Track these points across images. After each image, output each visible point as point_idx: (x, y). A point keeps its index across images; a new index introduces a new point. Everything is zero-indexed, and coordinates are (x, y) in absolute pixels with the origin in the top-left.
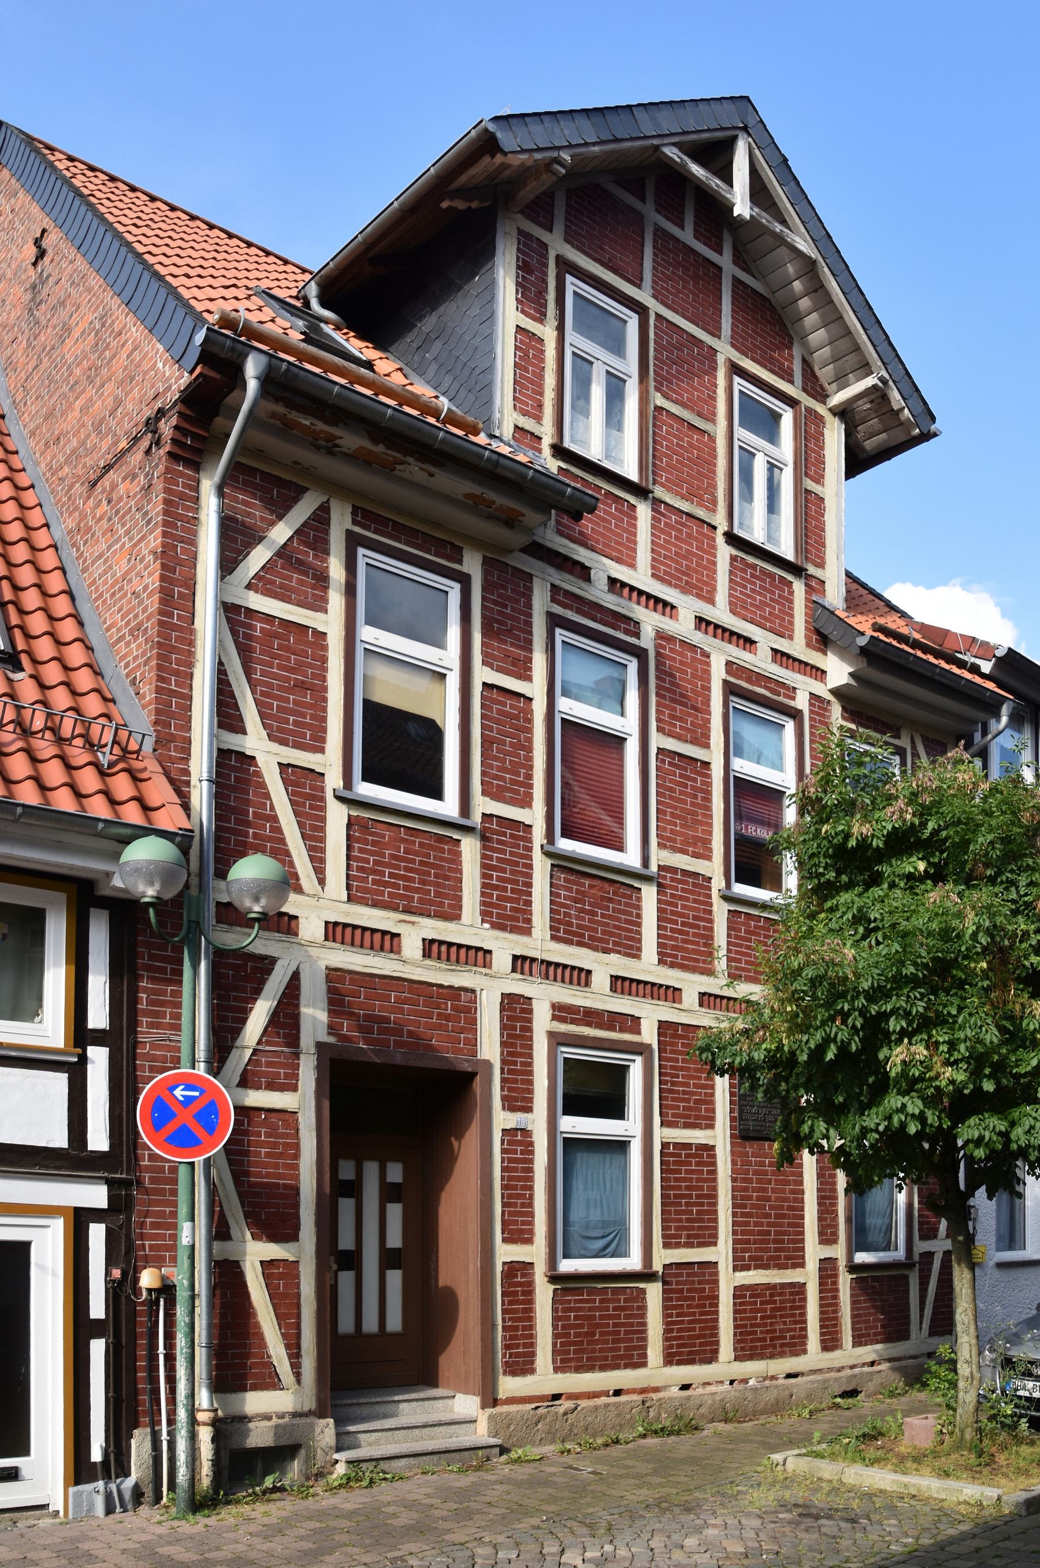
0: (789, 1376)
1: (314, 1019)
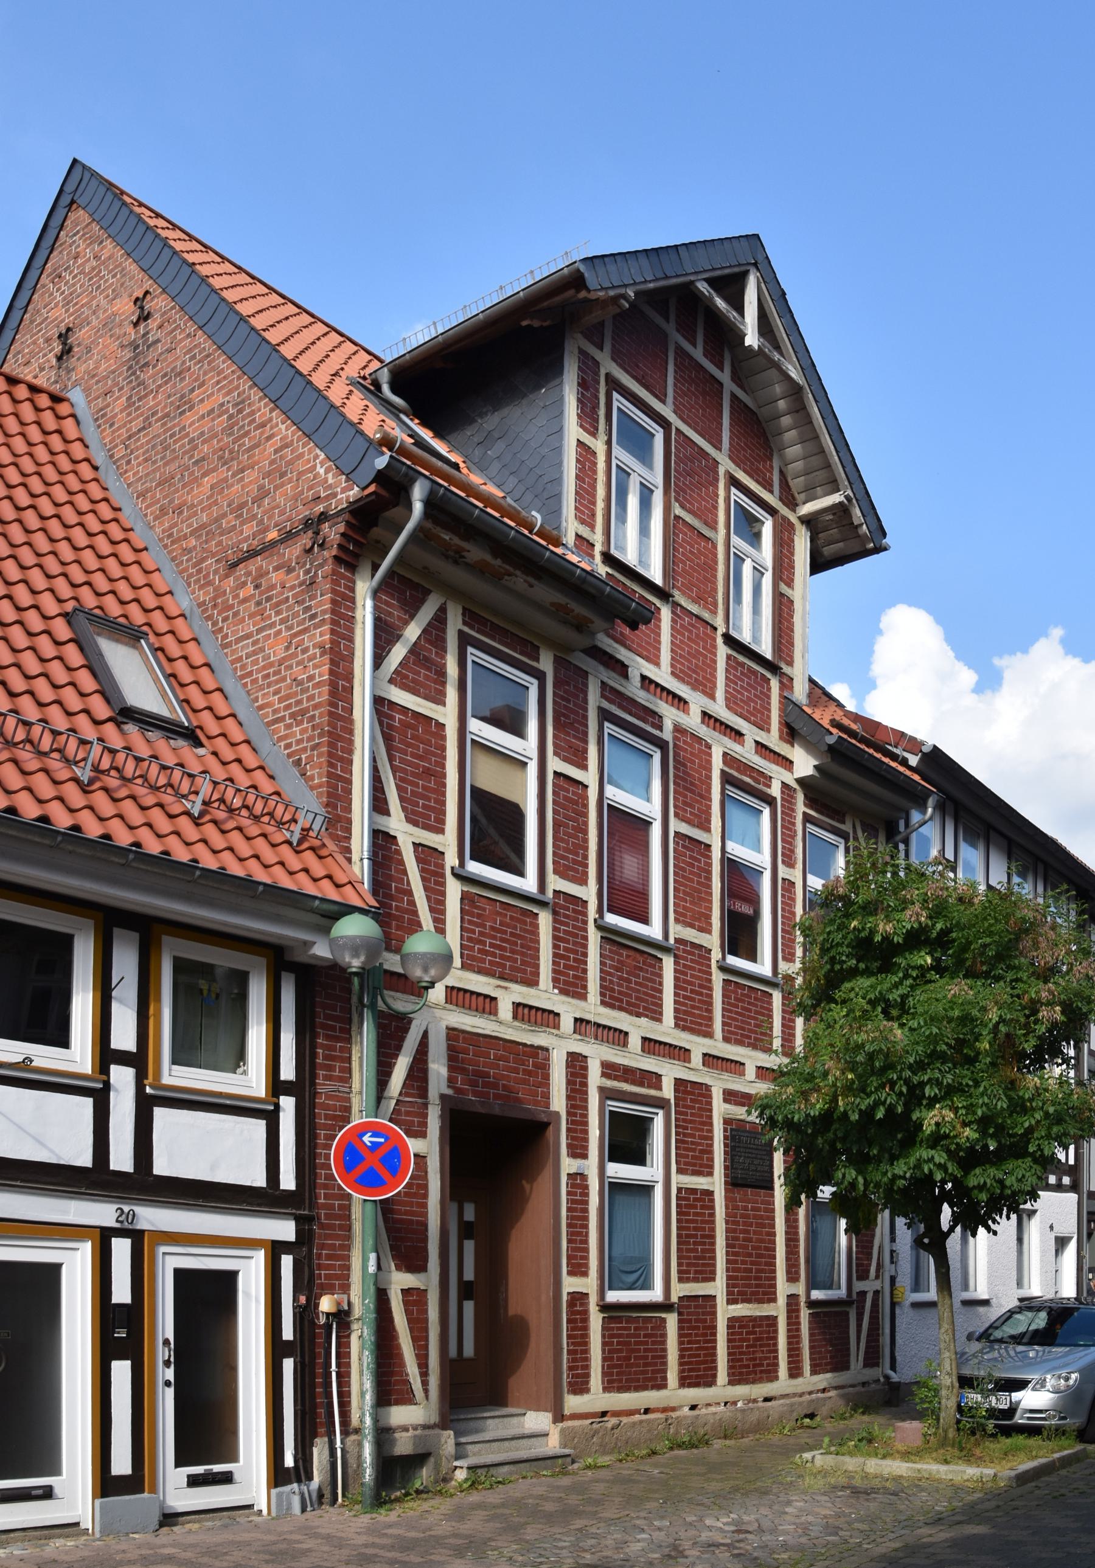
1: (438, 1073)
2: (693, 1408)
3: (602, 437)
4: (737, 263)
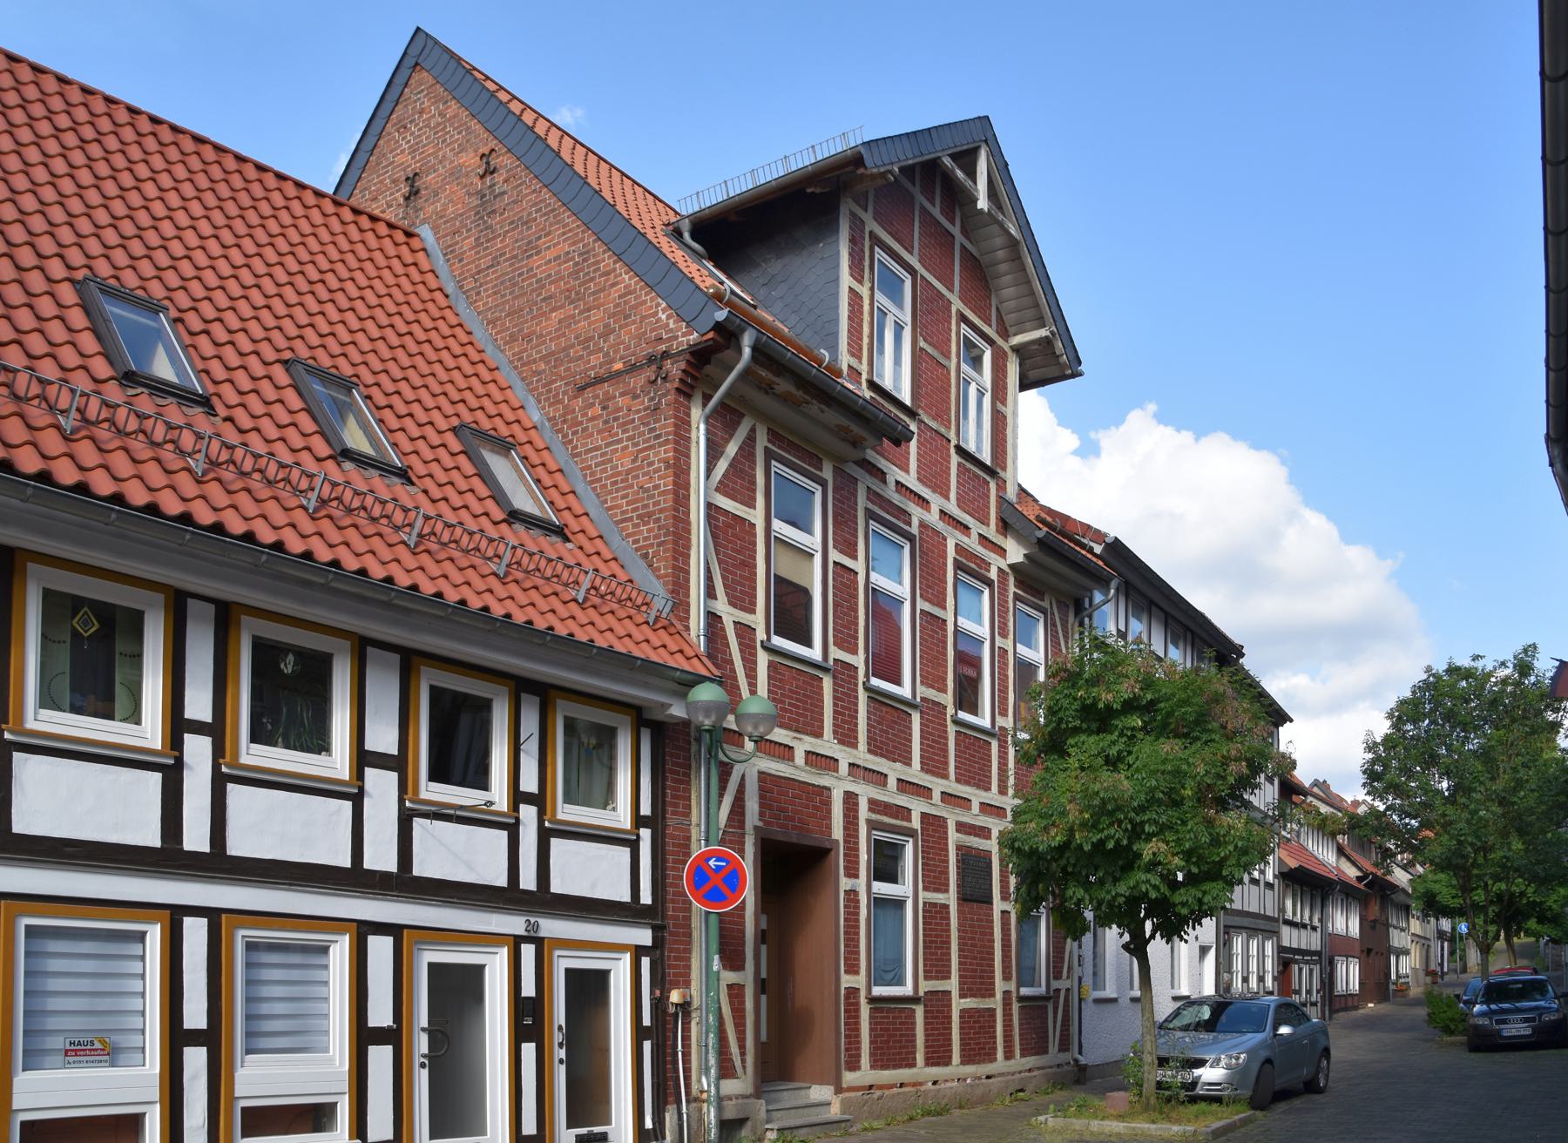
0: (988, 1077)
2: (935, 1083)
3: (867, 284)
4: (973, 140)
